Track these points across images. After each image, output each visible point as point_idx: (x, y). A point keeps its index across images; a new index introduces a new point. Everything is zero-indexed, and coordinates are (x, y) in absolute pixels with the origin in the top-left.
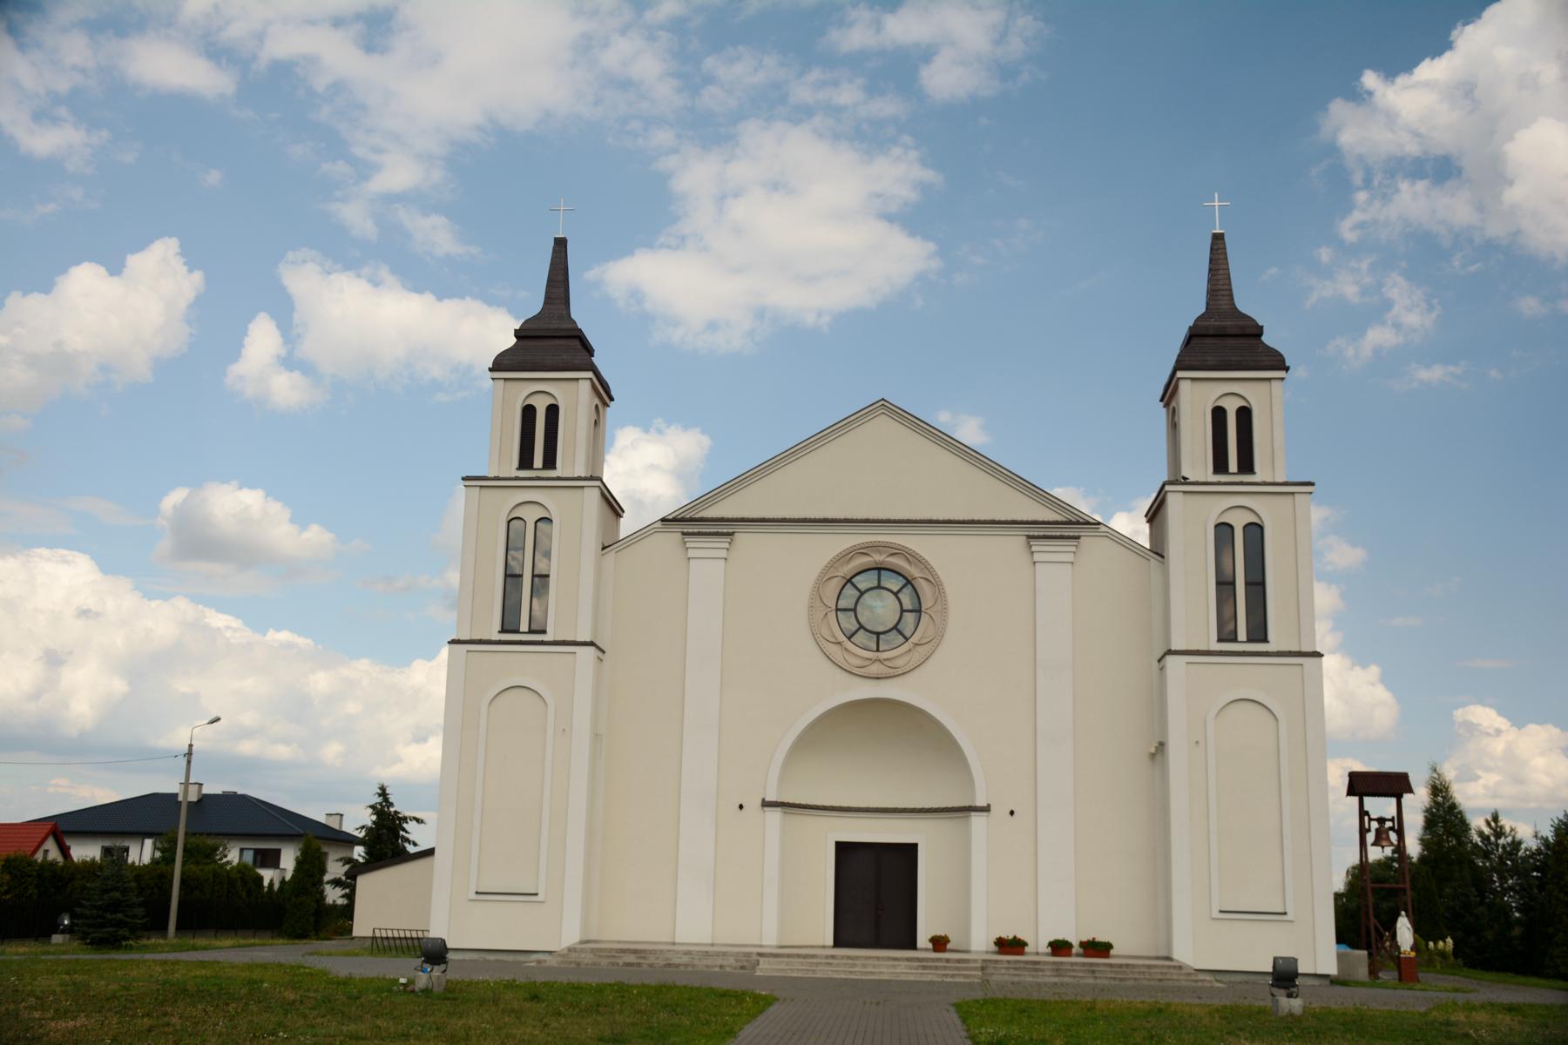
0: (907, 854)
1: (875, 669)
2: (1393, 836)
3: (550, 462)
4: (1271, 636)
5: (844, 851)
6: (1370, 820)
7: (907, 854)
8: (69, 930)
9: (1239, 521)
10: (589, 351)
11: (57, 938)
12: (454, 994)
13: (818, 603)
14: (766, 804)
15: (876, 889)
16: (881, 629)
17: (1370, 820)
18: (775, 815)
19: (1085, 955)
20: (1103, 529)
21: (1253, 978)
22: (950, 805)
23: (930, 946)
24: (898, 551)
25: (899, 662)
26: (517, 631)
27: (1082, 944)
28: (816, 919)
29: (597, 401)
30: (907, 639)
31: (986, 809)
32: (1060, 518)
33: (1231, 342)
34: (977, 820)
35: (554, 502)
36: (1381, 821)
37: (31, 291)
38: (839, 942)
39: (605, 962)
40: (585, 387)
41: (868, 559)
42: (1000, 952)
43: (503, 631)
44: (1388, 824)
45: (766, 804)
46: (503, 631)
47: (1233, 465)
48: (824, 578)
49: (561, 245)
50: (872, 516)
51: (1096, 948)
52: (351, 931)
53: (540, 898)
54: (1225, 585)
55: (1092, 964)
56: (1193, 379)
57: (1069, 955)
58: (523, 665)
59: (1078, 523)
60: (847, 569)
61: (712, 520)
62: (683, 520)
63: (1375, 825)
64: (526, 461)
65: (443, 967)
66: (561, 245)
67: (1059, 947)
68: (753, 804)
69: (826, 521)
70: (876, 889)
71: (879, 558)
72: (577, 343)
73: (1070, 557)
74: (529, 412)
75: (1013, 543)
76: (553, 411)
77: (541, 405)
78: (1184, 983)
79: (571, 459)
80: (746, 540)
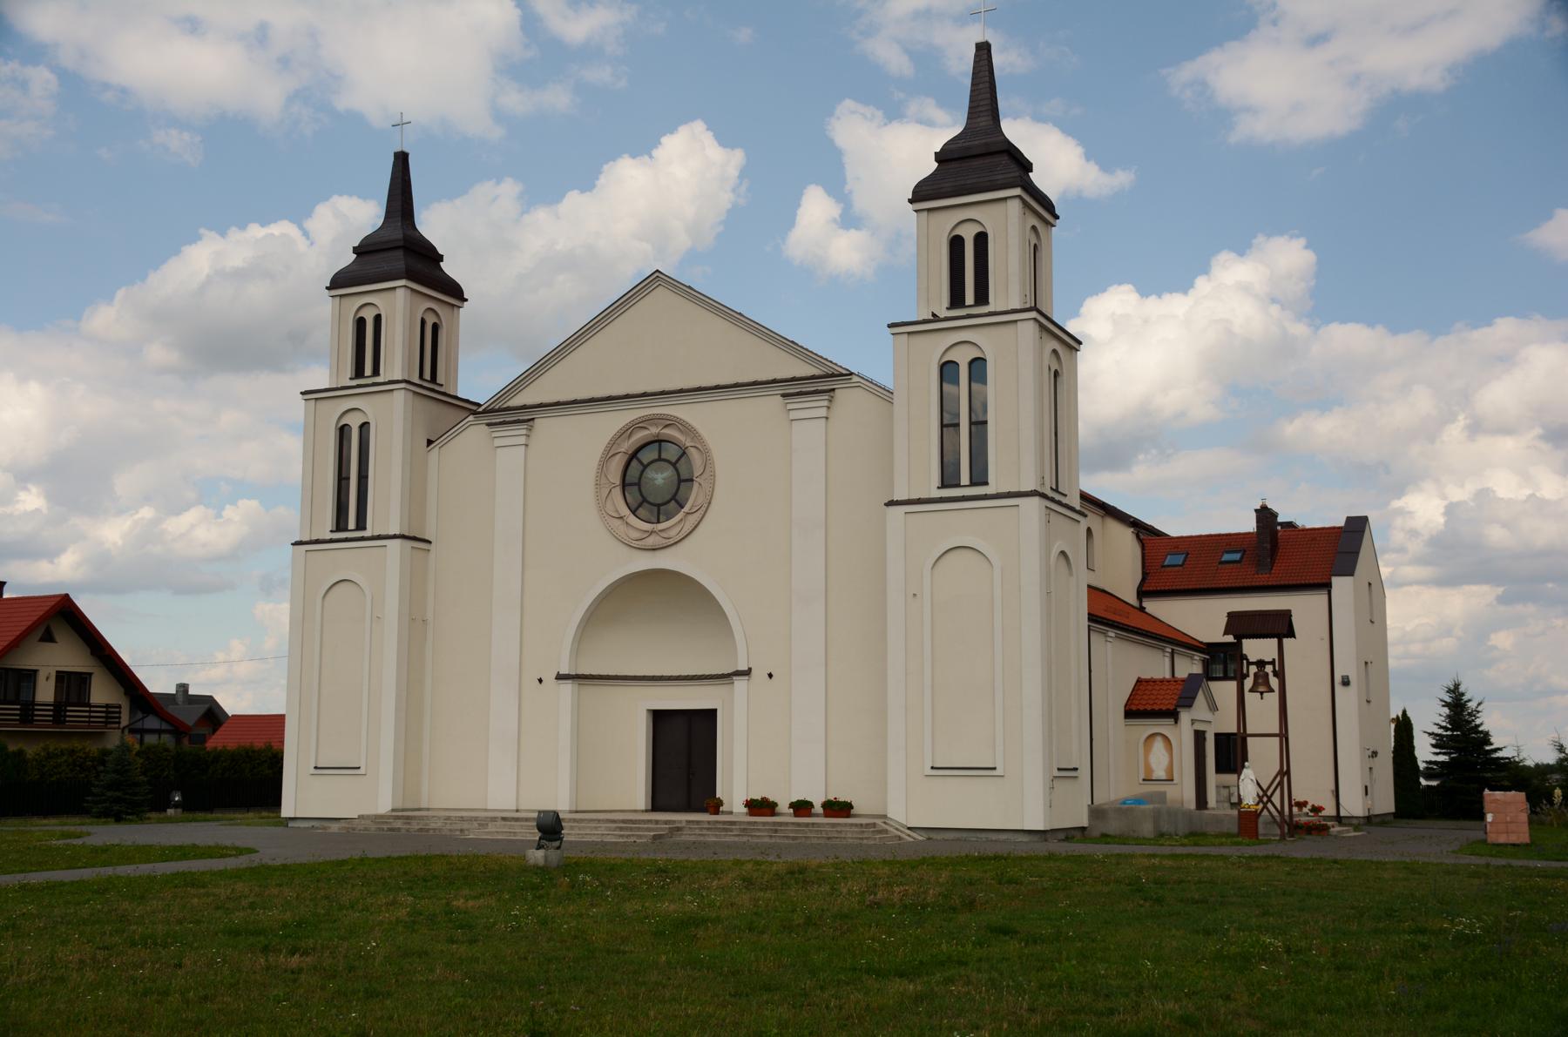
0: (707, 718)
1: (652, 541)
2: (1274, 682)
3: (982, 297)
4: (991, 479)
5: (660, 718)
6: (1249, 664)
7: (707, 718)
8: (177, 805)
9: (963, 357)
10: (1026, 166)
11: (170, 811)
12: (570, 868)
13: (604, 481)
14: (560, 677)
15: (684, 751)
16: (659, 501)
17: (1249, 664)
18: (567, 687)
19: (826, 815)
20: (855, 379)
21: (965, 835)
22: (707, 673)
23: (745, 810)
24: (671, 422)
25: (673, 533)
26: (958, 485)
27: (792, 805)
28: (626, 782)
29: (1034, 221)
30: (634, 512)
31: (748, 673)
32: (816, 372)
33: (976, 163)
34: (740, 683)
35: (988, 342)
36: (1261, 664)
37: (596, 173)
38: (656, 806)
39: (373, 827)
40: (1014, 207)
41: (646, 432)
42: (751, 813)
43: (943, 486)
44: (1269, 669)
45: (560, 677)
46: (943, 486)
47: (970, 298)
48: (608, 456)
49: (402, 160)
50: (650, 389)
51: (838, 809)
52: (277, 803)
53: (362, 771)
54: (948, 426)
55: (833, 825)
56: (929, 210)
57: (810, 815)
58: (348, 560)
59: (833, 375)
60: (628, 446)
61: (524, 407)
62: (493, 411)
63: (1253, 669)
64: (957, 299)
65: (557, 843)
66: (402, 160)
67: (801, 808)
68: (549, 677)
69: (700, 389)
70: (684, 751)
71: (654, 430)
72: (1005, 159)
73: (823, 412)
74: (956, 244)
75: (771, 403)
76: (981, 239)
77: (968, 233)
78: (815, 841)
79: (1007, 289)
80: (545, 425)
